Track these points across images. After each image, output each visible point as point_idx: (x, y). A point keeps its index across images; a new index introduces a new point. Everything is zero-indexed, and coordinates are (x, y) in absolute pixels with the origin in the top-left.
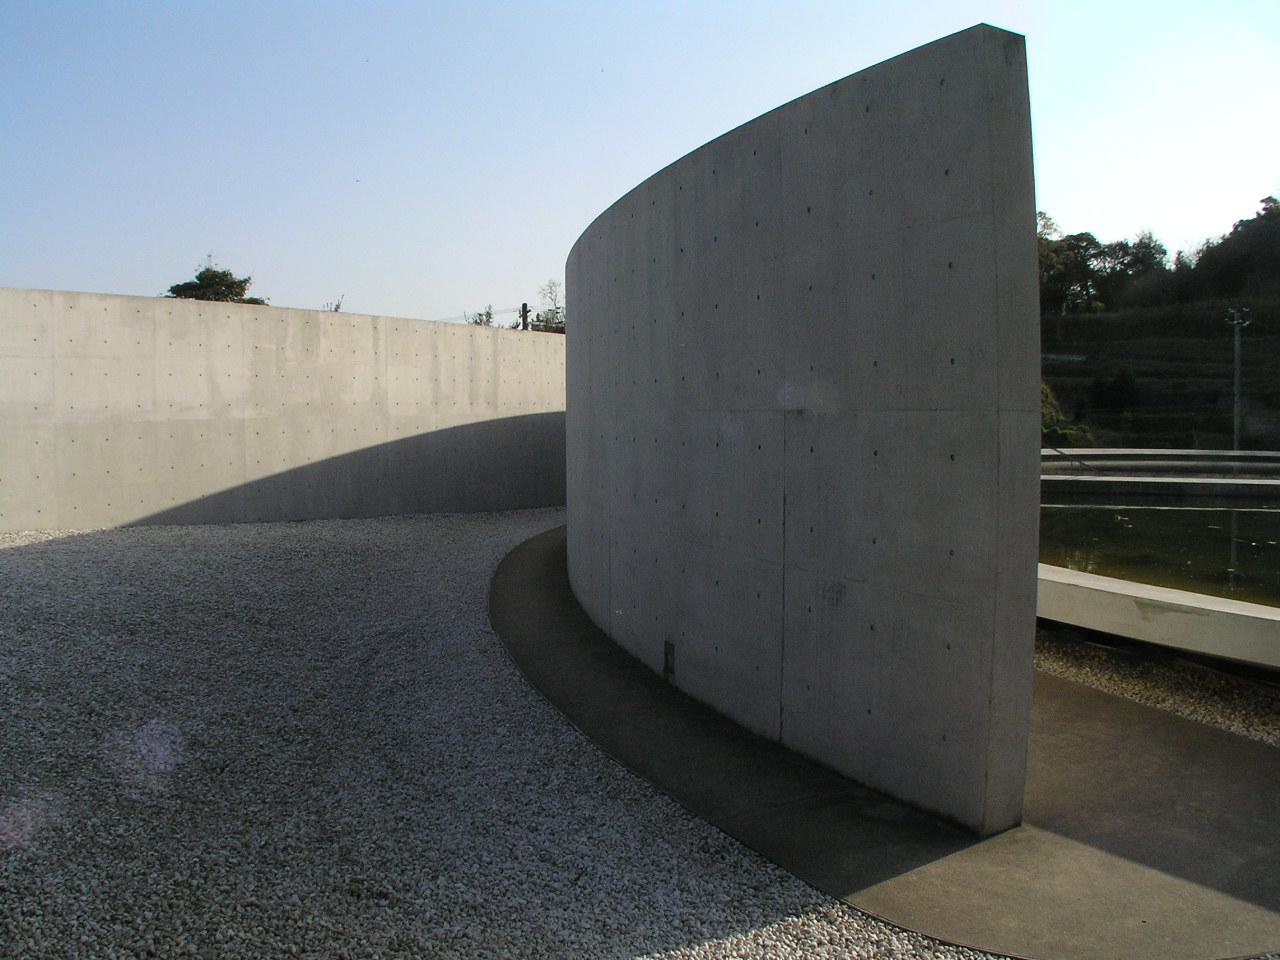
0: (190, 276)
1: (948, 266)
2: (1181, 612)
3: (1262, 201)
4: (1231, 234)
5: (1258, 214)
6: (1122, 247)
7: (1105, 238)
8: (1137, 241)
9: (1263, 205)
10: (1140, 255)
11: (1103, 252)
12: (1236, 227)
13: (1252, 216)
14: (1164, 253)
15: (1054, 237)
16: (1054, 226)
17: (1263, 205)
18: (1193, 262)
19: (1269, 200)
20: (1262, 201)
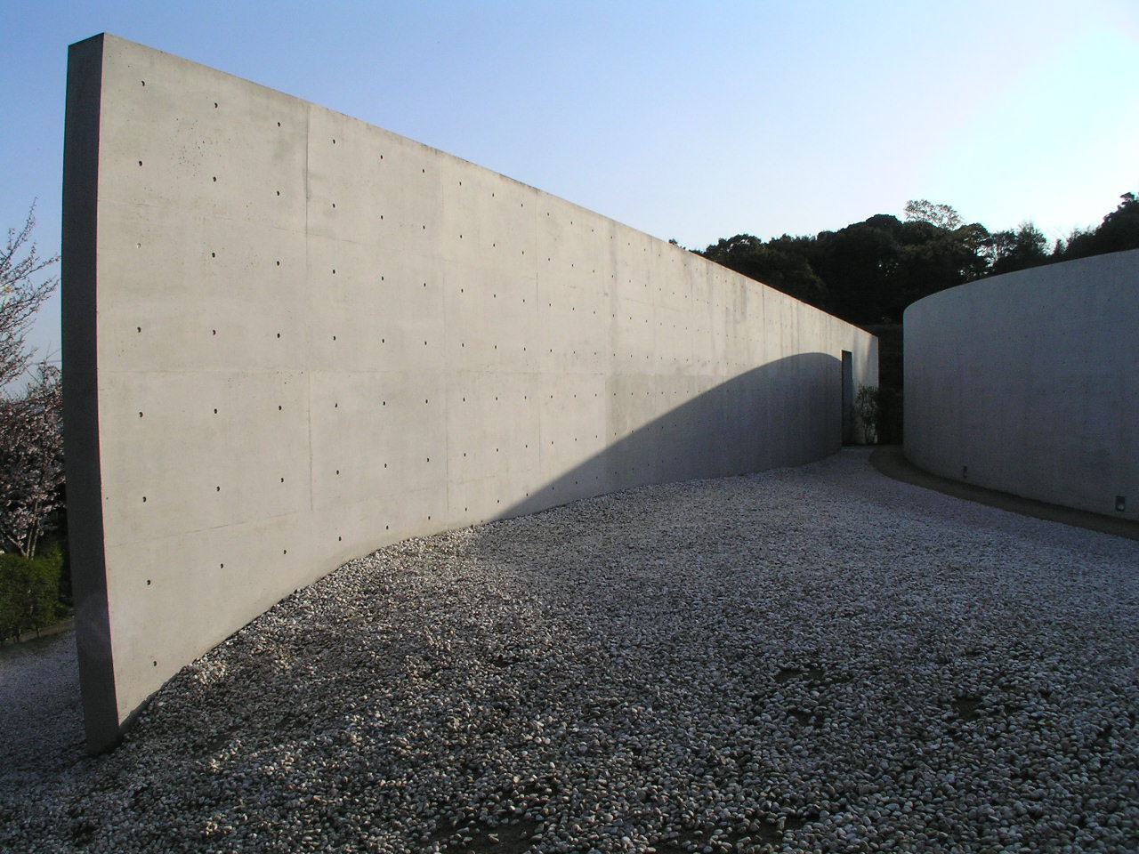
0: (693, 249)
1: (138, 164)
2: (1069, 510)
3: (1122, 196)
4: (1103, 225)
5: (1119, 207)
6: (1009, 236)
7: (993, 228)
8: (1020, 230)
9: (1123, 200)
10: (892, 260)
11: (990, 240)
12: (1106, 219)
13: (1115, 210)
14: (1044, 241)
15: (878, 386)
16: (958, 218)
17: (1123, 200)
18: (1065, 244)
19: (1129, 195)
20: (1122, 196)
